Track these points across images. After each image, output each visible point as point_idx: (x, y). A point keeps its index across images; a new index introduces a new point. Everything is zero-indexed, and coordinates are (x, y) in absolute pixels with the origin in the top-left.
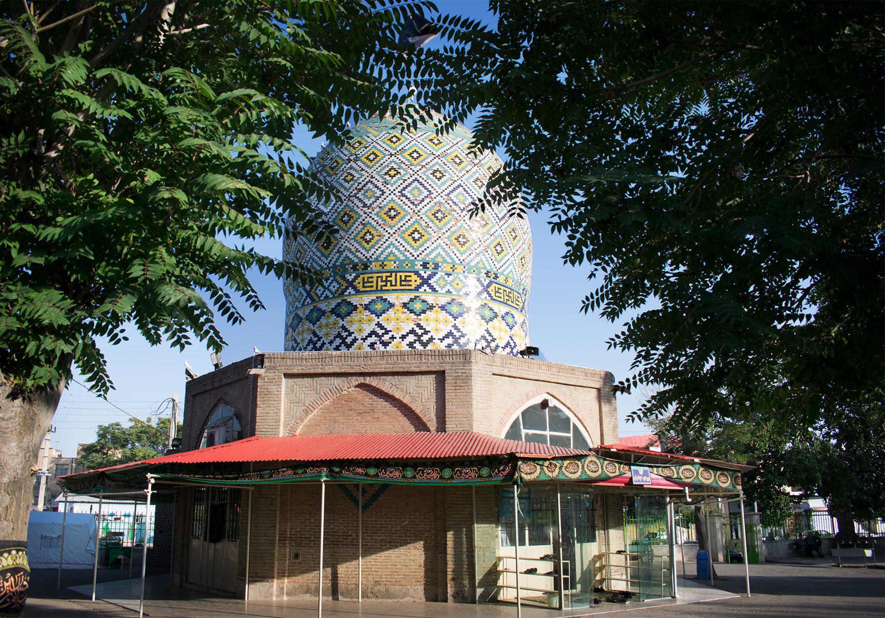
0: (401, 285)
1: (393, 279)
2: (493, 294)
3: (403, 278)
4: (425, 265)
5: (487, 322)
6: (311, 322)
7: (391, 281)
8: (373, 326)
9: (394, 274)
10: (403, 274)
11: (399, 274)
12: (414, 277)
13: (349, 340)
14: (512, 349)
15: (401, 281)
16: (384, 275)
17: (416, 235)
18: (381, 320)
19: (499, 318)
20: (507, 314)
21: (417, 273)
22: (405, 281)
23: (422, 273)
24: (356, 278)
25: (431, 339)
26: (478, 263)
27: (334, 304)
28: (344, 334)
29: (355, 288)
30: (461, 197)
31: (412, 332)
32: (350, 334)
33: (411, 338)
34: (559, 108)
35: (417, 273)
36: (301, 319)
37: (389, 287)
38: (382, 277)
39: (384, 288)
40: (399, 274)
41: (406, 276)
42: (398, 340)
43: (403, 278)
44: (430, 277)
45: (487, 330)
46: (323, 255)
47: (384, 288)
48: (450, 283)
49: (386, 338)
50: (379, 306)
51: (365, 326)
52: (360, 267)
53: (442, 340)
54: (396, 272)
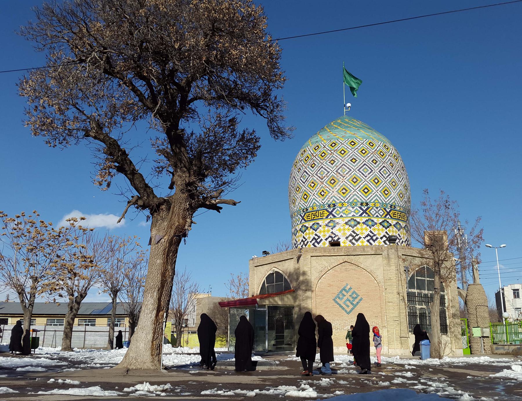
2: (392, 215)
4: (329, 206)
6: (302, 232)
10: (321, 211)
12: (326, 212)
17: (306, 197)
20: (396, 223)
21: (326, 210)
30: (385, 172)
31: (351, 235)
32: (306, 240)
33: (351, 238)
35: (326, 210)
37: (316, 218)
44: (332, 211)
48: (342, 212)
50: (315, 227)
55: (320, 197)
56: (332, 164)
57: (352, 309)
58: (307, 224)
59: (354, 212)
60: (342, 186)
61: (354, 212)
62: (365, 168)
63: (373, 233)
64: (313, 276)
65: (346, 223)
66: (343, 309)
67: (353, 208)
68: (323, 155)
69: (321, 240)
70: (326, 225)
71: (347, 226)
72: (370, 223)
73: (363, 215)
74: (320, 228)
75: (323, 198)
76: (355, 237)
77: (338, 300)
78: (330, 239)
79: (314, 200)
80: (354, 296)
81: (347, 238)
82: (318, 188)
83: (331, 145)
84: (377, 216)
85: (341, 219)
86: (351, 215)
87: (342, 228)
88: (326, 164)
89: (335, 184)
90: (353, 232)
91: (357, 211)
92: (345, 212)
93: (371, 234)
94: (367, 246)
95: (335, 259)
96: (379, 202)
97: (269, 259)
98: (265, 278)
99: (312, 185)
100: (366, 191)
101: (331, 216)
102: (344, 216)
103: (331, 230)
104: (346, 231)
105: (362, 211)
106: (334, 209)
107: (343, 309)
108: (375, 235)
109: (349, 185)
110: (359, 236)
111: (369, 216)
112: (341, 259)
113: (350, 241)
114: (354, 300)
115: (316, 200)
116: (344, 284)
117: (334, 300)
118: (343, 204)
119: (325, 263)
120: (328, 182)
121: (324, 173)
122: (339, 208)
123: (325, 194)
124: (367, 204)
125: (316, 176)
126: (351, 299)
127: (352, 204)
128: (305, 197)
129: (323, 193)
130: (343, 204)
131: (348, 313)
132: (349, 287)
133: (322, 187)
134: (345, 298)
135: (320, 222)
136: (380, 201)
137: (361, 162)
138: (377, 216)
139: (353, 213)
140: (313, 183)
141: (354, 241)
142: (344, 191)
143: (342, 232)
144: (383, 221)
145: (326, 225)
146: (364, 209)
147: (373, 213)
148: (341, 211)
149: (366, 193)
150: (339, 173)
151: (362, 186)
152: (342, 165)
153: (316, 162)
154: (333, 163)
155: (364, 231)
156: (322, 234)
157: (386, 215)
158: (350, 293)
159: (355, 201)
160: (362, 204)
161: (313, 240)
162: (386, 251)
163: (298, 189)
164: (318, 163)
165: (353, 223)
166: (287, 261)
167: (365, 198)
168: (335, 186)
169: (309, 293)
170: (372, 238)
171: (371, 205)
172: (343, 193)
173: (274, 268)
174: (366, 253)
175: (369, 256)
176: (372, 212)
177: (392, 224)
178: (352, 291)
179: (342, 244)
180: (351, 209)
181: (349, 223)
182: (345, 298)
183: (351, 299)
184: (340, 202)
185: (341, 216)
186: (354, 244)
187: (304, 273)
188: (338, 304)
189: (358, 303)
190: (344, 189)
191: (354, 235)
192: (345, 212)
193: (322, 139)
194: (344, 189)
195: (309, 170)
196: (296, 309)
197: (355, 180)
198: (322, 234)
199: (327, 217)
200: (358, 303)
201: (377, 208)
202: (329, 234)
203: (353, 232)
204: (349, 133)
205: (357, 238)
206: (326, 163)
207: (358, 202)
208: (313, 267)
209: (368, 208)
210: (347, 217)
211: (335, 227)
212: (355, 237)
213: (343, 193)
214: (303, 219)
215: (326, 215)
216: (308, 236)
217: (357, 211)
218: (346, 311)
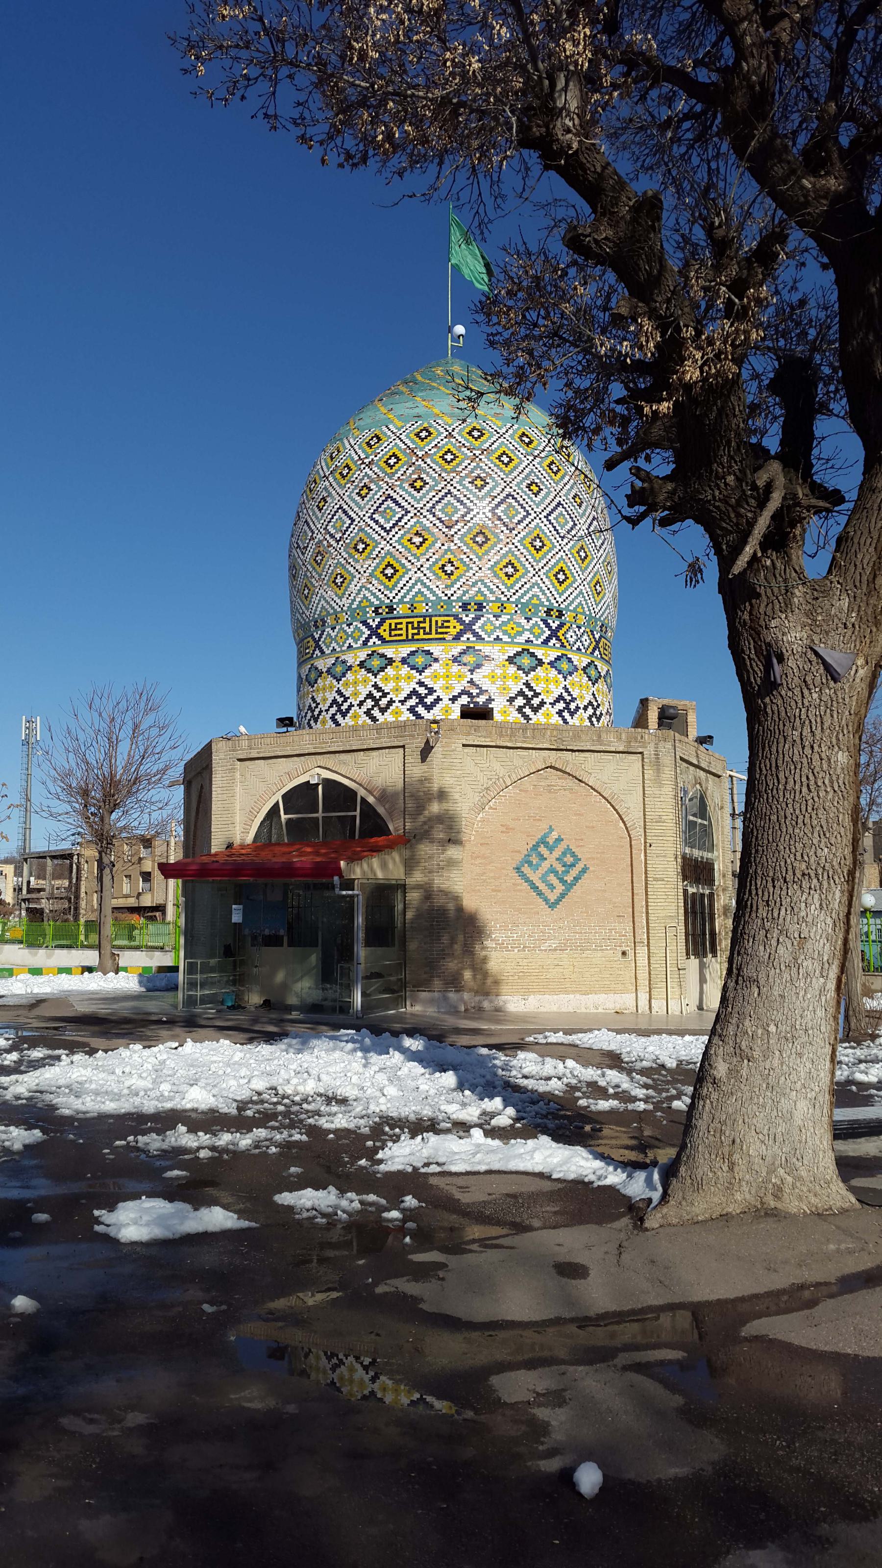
1: (427, 625)
4: (465, 607)
9: (428, 619)
10: (440, 619)
11: (434, 619)
12: (453, 622)
14: (595, 710)
15: (437, 627)
16: (415, 620)
17: (390, 572)
18: (379, 680)
19: (324, 675)
21: (456, 617)
22: (442, 627)
26: (577, 606)
27: (362, 655)
29: (380, 637)
30: (561, 520)
31: (521, 693)
32: (346, 699)
33: (520, 701)
34: (576, 431)
35: (456, 617)
37: (422, 636)
39: (416, 637)
41: (396, 624)
46: (386, 587)
47: (416, 637)
48: (500, 627)
49: (520, 701)
50: (420, 660)
51: (360, 688)
52: (383, 610)
54: (431, 617)
55: (439, 578)
56: (480, 489)
57: (563, 896)
59: (531, 630)
60: (505, 556)
61: (531, 630)
63: (570, 694)
64: (464, 803)
66: (540, 894)
67: (528, 619)
69: (438, 700)
70: (455, 660)
71: (512, 669)
74: (435, 666)
75: (449, 582)
76: (529, 700)
77: (526, 869)
78: (464, 700)
79: (419, 586)
80: (569, 859)
81: (511, 700)
82: (436, 551)
83: (417, 435)
85: (497, 647)
86: (522, 639)
87: (499, 672)
88: (463, 488)
89: (486, 547)
90: (527, 685)
91: (536, 631)
92: (508, 628)
93: (526, 690)
94: (556, 727)
95: (521, 757)
96: (583, 613)
97: (301, 740)
98: (278, 797)
99: (417, 540)
100: (561, 577)
101: (469, 635)
102: (505, 638)
103: (469, 676)
104: (510, 683)
106: (478, 618)
107: (540, 894)
109: (524, 555)
110: (435, 696)
111: (563, 646)
112: (539, 759)
113: (520, 710)
115: (421, 585)
116: (544, 826)
117: (518, 869)
118: (503, 607)
119: (497, 766)
120: (467, 539)
121: (456, 510)
122: (491, 616)
123: (457, 573)
124: (560, 614)
125: (430, 517)
126: (560, 869)
127: (527, 610)
129: (449, 568)
130: (503, 607)
131: (553, 906)
132: (555, 835)
133: (449, 549)
134: (546, 865)
135: (436, 649)
136: (373, 600)
137: (551, 497)
138: (579, 649)
139: (527, 635)
140: (417, 534)
141: (527, 710)
142: (510, 570)
143: (498, 683)
144: (558, 658)
145: (455, 660)
146: (554, 626)
147: (572, 640)
148: (498, 623)
150: (500, 519)
151: (553, 561)
152: (508, 496)
153: (428, 474)
154: (483, 487)
155: (552, 687)
158: (557, 853)
159: (535, 601)
160: (548, 612)
162: (652, 745)
163: (362, 546)
164: (434, 479)
165: (524, 660)
166: (375, 753)
167: (558, 600)
168: (487, 553)
169: (453, 852)
170: (528, 700)
171: (568, 617)
172: (506, 574)
173: (318, 770)
174: (603, 748)
175: (609, 756)
178: (562, 847)
179: (497, 716)
180: (523, 621)
181: (517, 660)
182: (546, 865)
183: (560, 869)
184: (498, 600)
185: (498, 639)
186: (527, 718)
187: (442, 795)
188: (527, 880)
189: (577, 879)
190: (510, 563)
191: (530, 694)
192: (508, 628)
193: (436, 411)
194: (510, 563)
195: (403, 493)
196: (414, 896)
197: (538, 545)
199: (457, 638)
200: (577, 879)
201: (579, 627)
202: (463, 684)
203: (527, 685)
204: (403, 408)
205: (536, 702)
206: (459, 482)
208: (465, 776)
210: (512, 643)
211: (479, 666)
212: (529, 700)
213: (506, 574)
215: (453, 632)
218: (546, 900)
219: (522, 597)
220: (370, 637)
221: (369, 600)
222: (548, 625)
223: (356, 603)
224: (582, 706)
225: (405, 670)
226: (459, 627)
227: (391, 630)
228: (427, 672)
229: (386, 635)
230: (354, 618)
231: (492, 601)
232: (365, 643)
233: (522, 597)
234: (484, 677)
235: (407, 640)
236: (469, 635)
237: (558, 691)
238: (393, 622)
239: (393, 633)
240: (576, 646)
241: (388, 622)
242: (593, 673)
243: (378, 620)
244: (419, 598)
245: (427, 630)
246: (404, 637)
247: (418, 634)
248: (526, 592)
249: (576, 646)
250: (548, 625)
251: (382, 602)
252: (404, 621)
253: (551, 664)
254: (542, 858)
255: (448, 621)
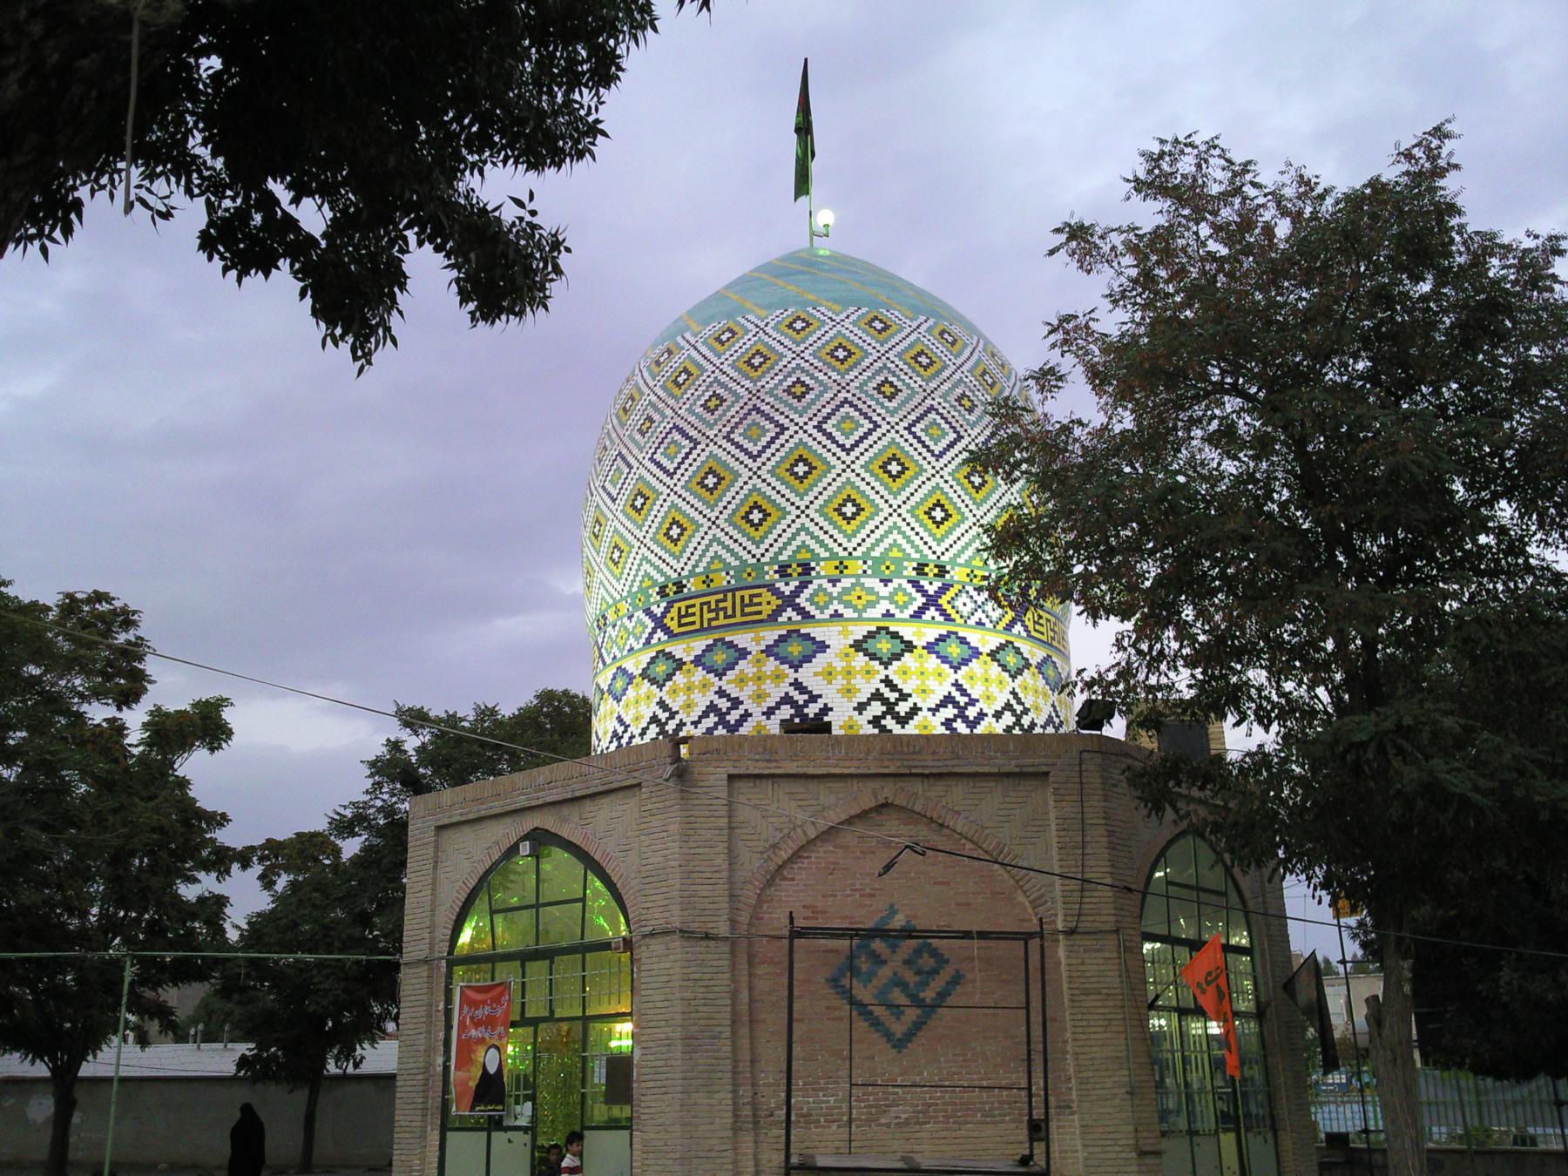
0: (743, 614)
1: (728, 604)
2: (1030, 625)
3: (747, 601)
4: (783, 571)
5: (1013, 677)
6: (653, 681)
7: (717, 618)
8: (786, 688)
10: (746, 593)
12: (767, 595)
13: (903, 708)
15: (743, 606)
16: (713, 599)
21: (771, 587)
22: (751, 604)
23: (780, 585)
24: (667, 610)
25: (915, 710)
28: (663, 716)
31: (877, 696)
32: (673, 715)
33: (877, 708)
35: (771, 587)
36: (631, 678)
37: (722, 621)
38: (708, 603)
40: (738, 594)
41: (751, 596)
42: (990, 720)
43: (747, 601)
44: (797, 592)
45: (1014, 693)
53: (934, 711)
54: (733, 591)
57: (918, 1026)
58: (678, 649)
61: (890, 598)
62: (934, 423)
65: (858, 646)
67: (886, 582)
68: (756, 361)
69: (746, 715)
71: (860, 660)
72: (720, 658)
73: (927, 616)
78: (786, 712)
81: (861, 708)
84: (980, 623)
85: (836, 628)
91: (900, 598)
92: (853, 597)
104: (859, 682)
105: (920, 600)
106: (803, 586)
108: (973, 702)
110: (741, 711)
111: (948, 618)
114: (924, 985)
117: (834, 981)
118: (841, 567)
124: (942, 571)
128: (675, 532)
131: (900, 1044)
135: (742, 639)
137: (918, 399)
138: (980, 623)
140: (711, 471)
144: (1002, 647)
146: (931, 590)
147: (965, 611)
148: (835, 591)
149: (938, 524)
152: (842, 404)
154: (803, 395)
156: (751, 688)
157: (1012, 623)
159: (895, 553)
160: (920, 569)
161: (705, 714)
166: (604, 802)
170: (962, 710)
176: (958, 603)
177: (1033, 662)
180: (879, 587)
181: (967, 653)
182: (885, 972)
183: (910, 977)
184: (834, 556)
185: (837, 615)
191: (893, 696)
192: (853, 597)
198: (751, 688)
200: (942, 995)
207: (908, 558)
209: (945, 588)
210: (860, 619)
214: (660, 623)
215: (767, 610)
216: (632, 712)
217: (900, 598)
218: (888, 1035)
219: (872, 548)
220: (654, 631)
221: (651, 578)
222: (920, 589)
223: (637, 584)
224: (991, 712)
225: (771, 664)
226: (776, 602)
227: (680, 617)
228: (731, 675)
229: (673, 625)
230: (636, 608)
231: (824, 559)
232: (648, 641)
233: (872, 548)
234: (816, 674)
235: (702, 630)
236: (790, 613)
237: (943, 689)
238: (683, 605)
239: (684, 621)
240: (974, 619)
241: (677, 605)
242: (1011, 660)
243: (664, 605)
244: (717, 565)
245: (730, 612)
246: (697, 626)
247: (717, 618)
248: (881, 540)
249: (974, 619)
250: (920, 589)
251: (668, 577)
252: (697, 602)
253: (930, 648)
254: (879, 961)
255: (759, 595)
